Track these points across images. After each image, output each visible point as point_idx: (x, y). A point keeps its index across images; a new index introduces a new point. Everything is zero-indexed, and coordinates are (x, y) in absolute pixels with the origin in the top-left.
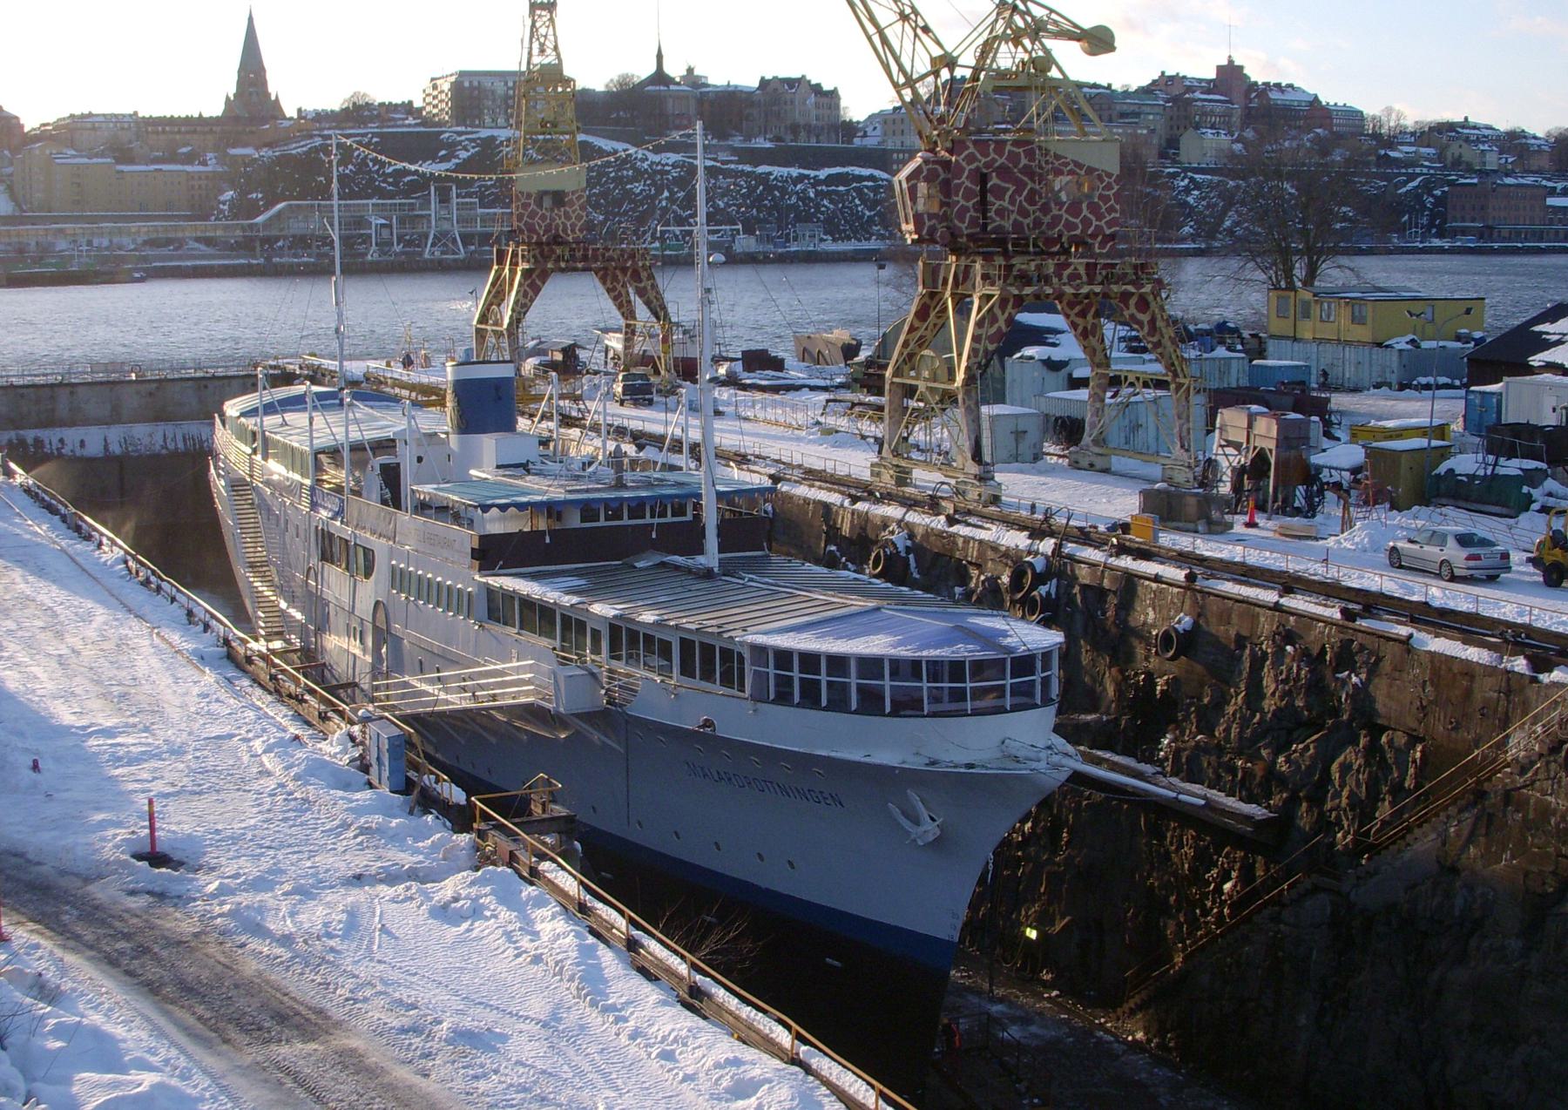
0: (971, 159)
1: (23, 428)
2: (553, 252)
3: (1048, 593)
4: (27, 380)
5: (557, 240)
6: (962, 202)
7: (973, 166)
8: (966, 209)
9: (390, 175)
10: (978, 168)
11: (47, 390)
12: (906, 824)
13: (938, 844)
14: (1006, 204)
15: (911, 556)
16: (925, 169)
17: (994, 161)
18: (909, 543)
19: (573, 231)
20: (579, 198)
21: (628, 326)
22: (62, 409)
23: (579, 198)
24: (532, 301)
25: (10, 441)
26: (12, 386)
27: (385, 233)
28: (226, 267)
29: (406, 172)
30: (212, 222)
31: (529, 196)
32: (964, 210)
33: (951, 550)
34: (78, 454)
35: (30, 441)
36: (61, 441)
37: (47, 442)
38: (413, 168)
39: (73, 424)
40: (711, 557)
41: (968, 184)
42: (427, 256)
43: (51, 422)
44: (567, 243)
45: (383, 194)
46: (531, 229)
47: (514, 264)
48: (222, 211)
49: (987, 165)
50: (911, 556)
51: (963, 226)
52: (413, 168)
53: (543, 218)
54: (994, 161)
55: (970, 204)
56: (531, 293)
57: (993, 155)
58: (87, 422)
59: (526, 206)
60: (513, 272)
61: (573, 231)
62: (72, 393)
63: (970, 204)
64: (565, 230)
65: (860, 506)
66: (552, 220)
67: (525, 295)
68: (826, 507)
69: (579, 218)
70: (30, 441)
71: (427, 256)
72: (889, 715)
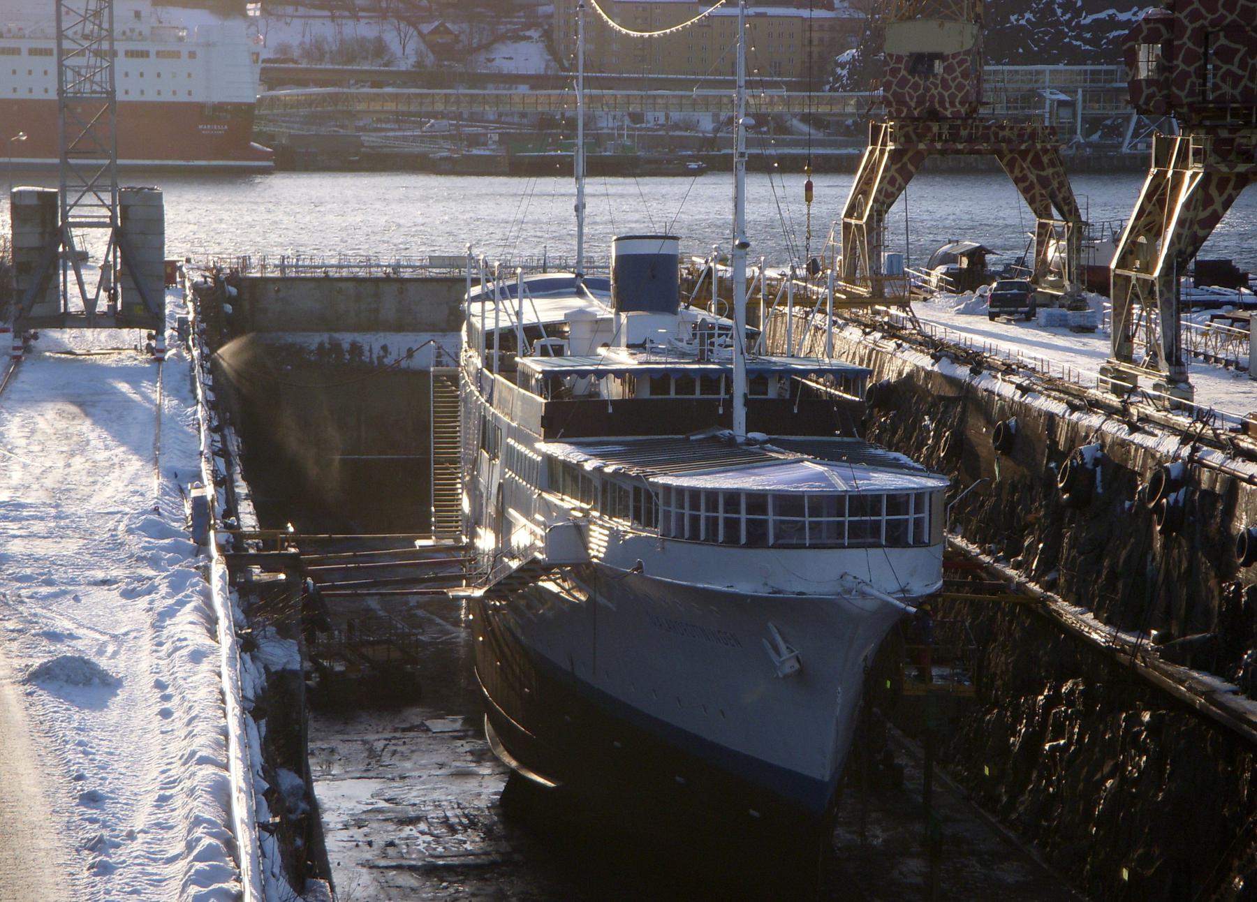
0: (1195, 16)
1: (336, 330)
2: (929, 129)
3: (1176, 501)
4: (345, 273)
5: (934, 115)
6: (1182, 66)
7: (1197, 25)
8: (1188, 75)
9: (1088, 28)
10: (1203, 26)
11: (350, 285)
12: (772, 654)
13: (802, 676)
14: (1234, 69)
15: (1099, 469)
16: (1145, 28)
17: (1223, 17)
18: (1099, 454)
19: (952, 104)
20: (961, 63)
21: (1041, 226)
22: (389, 309)
23: (961, 63)
24: (900, 189)
25: (321, 345)
26: (327, 278)
27: (1065, 113)
28: (827, 158)
29: (1112, 24)
30: (826, 93)
31: (899, 59)
32: (1185, 75)
33: (1126, 461)
34: (404, 364)
35: (346, 346)
36: (384, 348)
37: (366, 348)
38: (1123, 17)
39: (399, 328)
40: (739, 428)
41: (1190, 45)
42: (1125, 149)
43: (374, 325)
44: (946, 118)
45: (1075, 57)
46: (901, 102)
47: (884, 144)
48: (839, 78)
49: (1213, 23)
50: (1099, 469)
51: (1183, 94)
52: (1123, 17)
53: (915, 87)
54: (1223, 17)
55: (1192, 69)
56: (899, 180)
57: (1221, 11)
58: (416, 327)
59: (894, 72)
60: (882, 152)
61: (952, 104)
62: (401, 292)
63: (1192, 69)
64: (942, 103)
65: (1076, 416)
66: (927, 89)
67: (892, 182)
68: (1051, 417)
69: (960, 87)
70: (346, 346)
71: (1125, 149)
72: (744, 546)
